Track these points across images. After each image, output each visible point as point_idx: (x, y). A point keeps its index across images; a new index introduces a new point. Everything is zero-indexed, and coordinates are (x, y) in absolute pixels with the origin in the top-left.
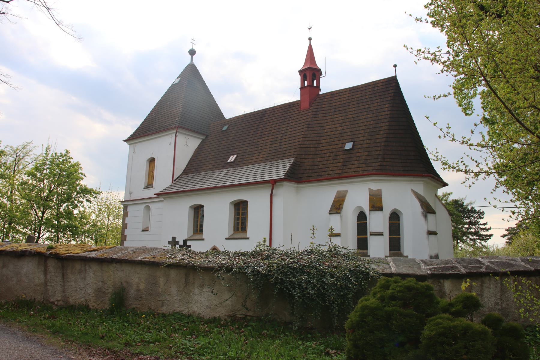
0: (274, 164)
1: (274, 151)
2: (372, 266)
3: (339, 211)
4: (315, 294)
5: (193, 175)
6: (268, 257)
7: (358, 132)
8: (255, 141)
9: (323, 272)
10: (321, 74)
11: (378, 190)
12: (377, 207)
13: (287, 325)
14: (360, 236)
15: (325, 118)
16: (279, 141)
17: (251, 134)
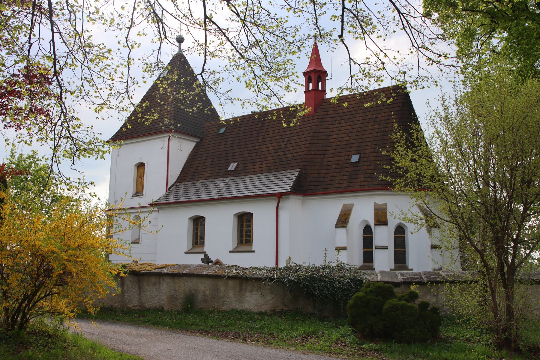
0: (279, 175)
1: (278, 161)
2: (366, 276)
3: (345, 225)
4: (329, 293)
6: (296, 271)
8: (257, 147)
9: (334, 280)
10: (327, 75)
11: (383, 204)
12: (382, 222)
14: (366, 250)
15: (331, 126)
16: (283, 150)
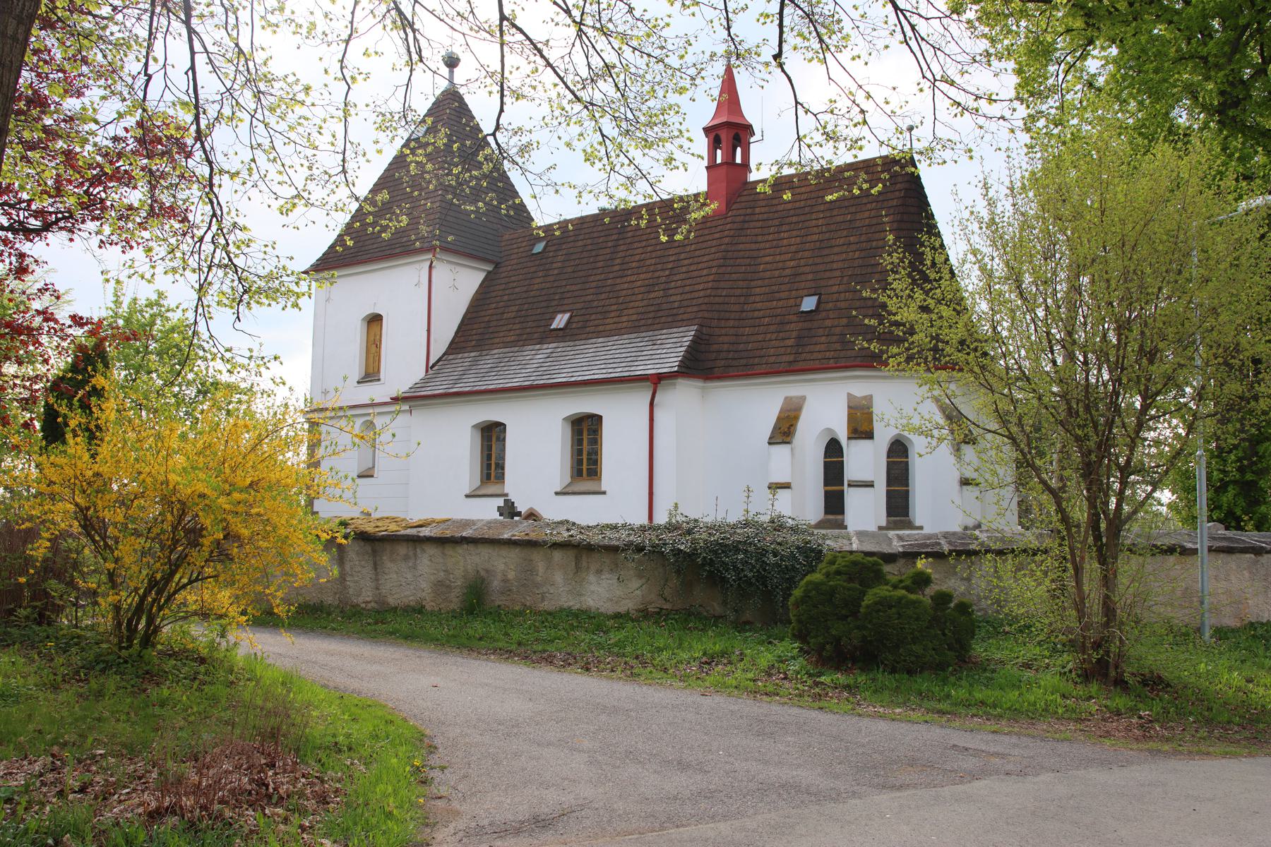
1: (652, 308)
2: (828, 542)
3: (788, 440)
5: (472, 354)
6: (689, 532)
7: (828, 274)
8: (609, 282)
10: (753, 134)
11: (865, 397)
13: (717, 619)
14: (829, 488)
15: (760, 239)
16: (662, 286)
17: (600, 264)
